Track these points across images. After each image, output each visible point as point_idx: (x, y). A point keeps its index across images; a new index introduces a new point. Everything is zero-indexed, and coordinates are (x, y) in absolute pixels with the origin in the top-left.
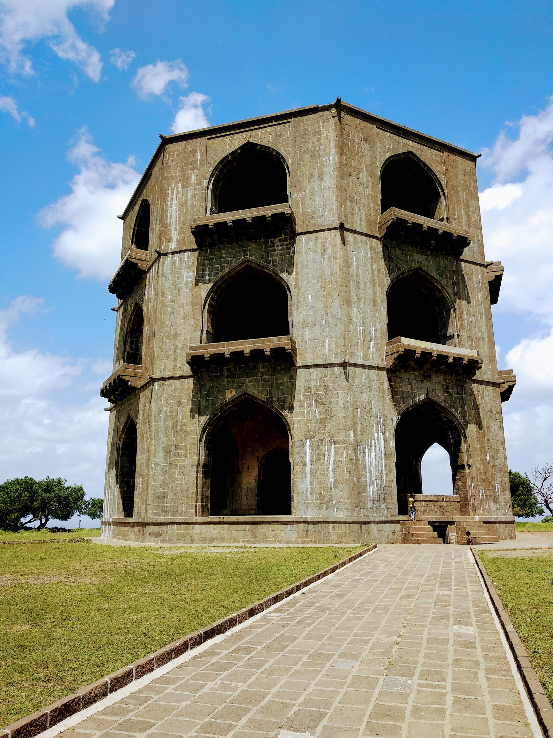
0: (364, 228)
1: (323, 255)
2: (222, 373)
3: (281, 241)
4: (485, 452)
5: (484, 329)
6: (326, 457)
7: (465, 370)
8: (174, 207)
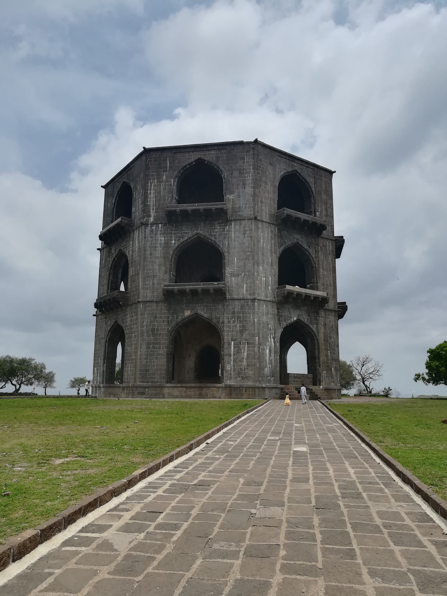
0: (267, 218)
1: (244, 234)
3: (219, 223)
5: (331, 278)
6: (242, 351)
7: (321, 303)
8: (152, 195)
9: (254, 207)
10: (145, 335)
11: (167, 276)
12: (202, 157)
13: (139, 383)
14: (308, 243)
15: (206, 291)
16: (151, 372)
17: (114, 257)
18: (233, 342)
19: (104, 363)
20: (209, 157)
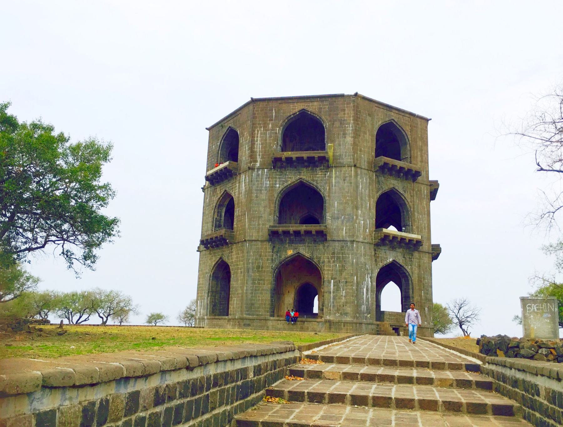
1: (344, 180)
2: (286, 241)
3: (321, 169)
4: (422, 290)
8: (259, 142)
9: (353, 156)
10: (251, 271)
11: (271, 217)
12: (306, 108)
13: (245, 316)
14: (403, 188)
15: (308, 233)
16: (256, 305)
17: (219, 197)
18: (332, 281)
19: (208, 296)
20: (313, 108)
